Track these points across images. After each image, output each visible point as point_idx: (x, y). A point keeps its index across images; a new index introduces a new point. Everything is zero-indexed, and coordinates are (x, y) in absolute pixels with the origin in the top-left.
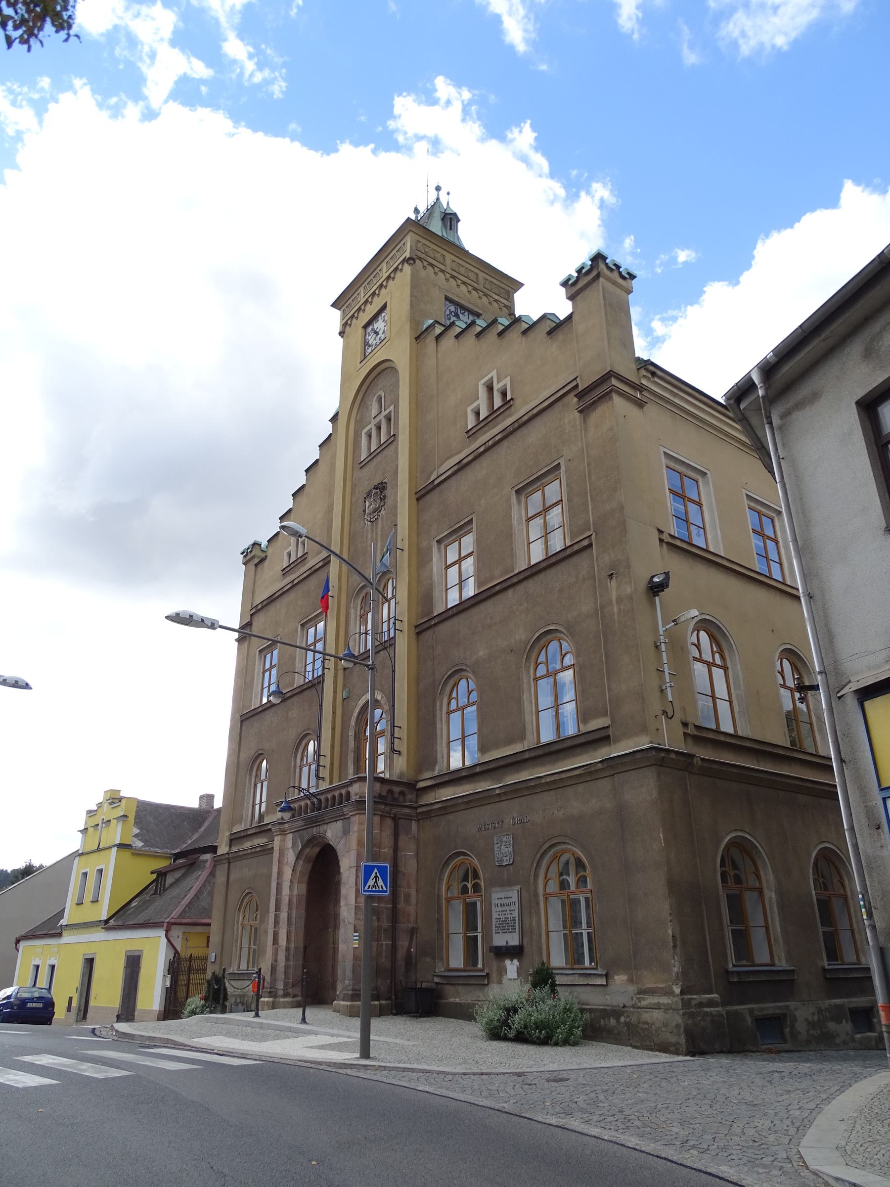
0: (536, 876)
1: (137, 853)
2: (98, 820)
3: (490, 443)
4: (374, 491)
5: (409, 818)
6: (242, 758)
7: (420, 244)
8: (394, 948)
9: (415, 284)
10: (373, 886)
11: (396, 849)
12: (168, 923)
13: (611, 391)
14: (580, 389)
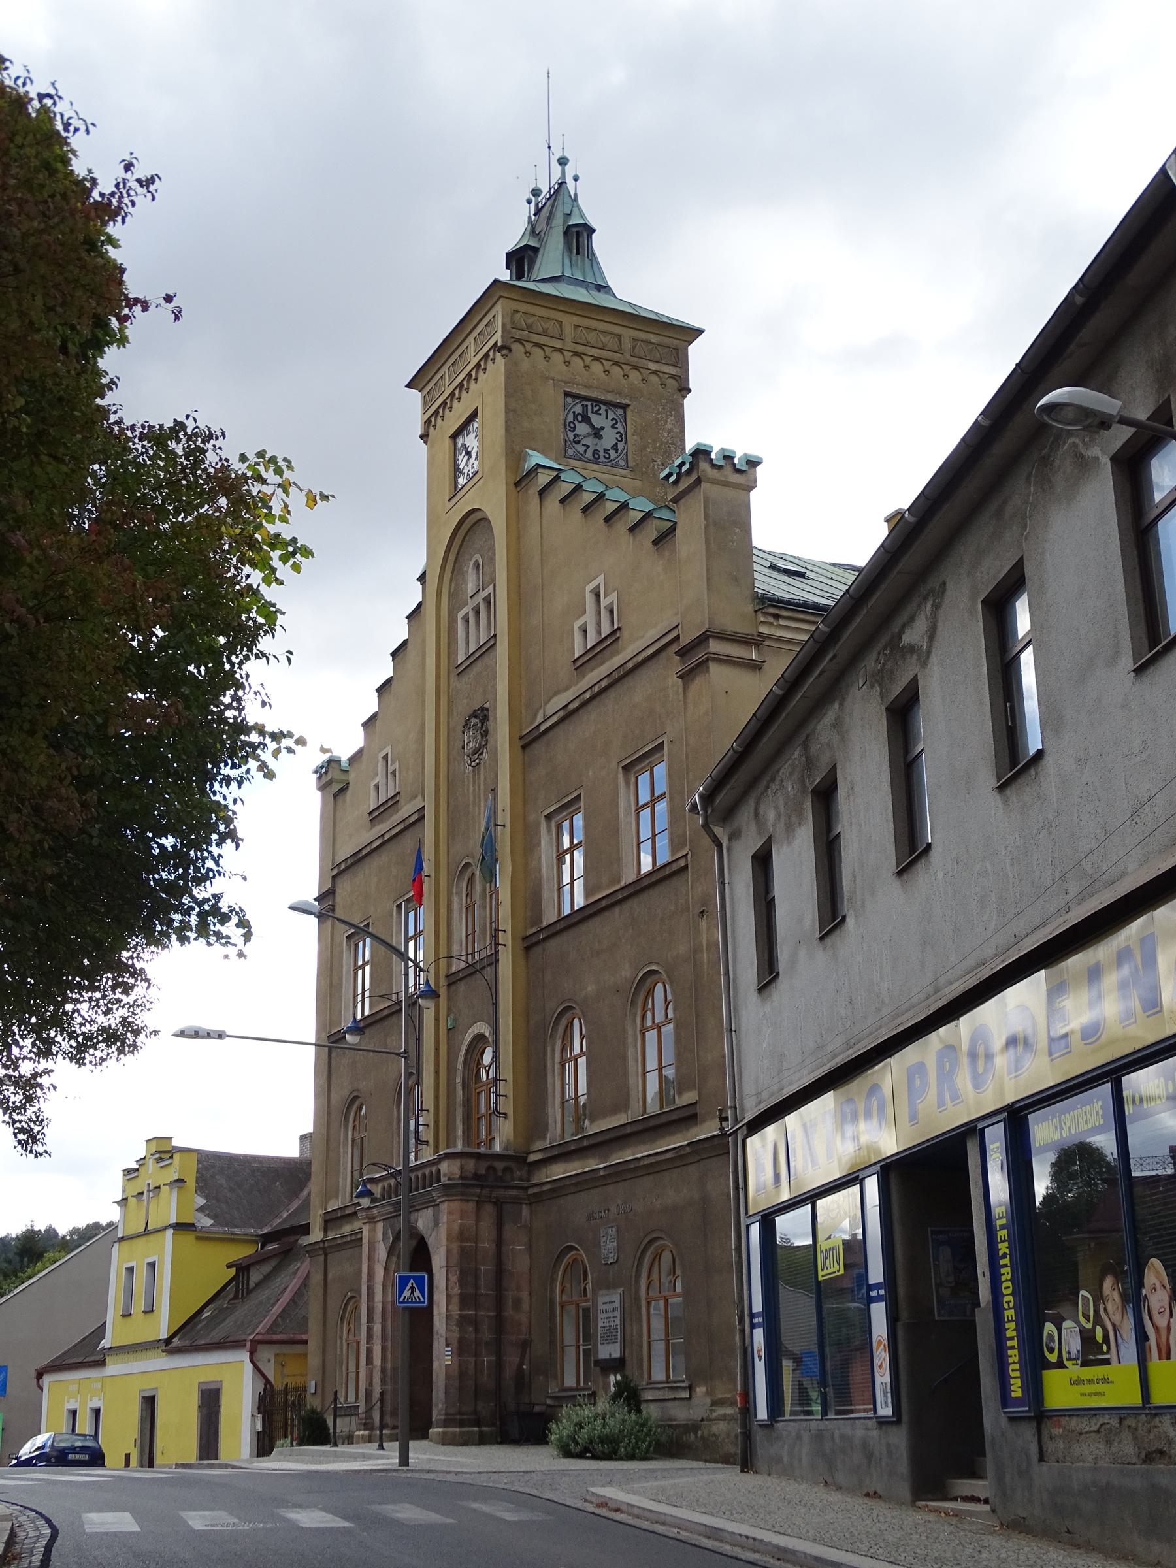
0: (638, 1276)
1: (205, 1237)
2: (141, 1185)
3: (588, 695)
4: (474, 721)
5: (517, 1201)
6: (333, 1102)
7: (518, 316)
8: (499, 1365)
9: (513, 389)
10: (410, 1297)
11: (499, 1242)
12: (251, 1341)
13: (707, 660)
14: (684, 641)
